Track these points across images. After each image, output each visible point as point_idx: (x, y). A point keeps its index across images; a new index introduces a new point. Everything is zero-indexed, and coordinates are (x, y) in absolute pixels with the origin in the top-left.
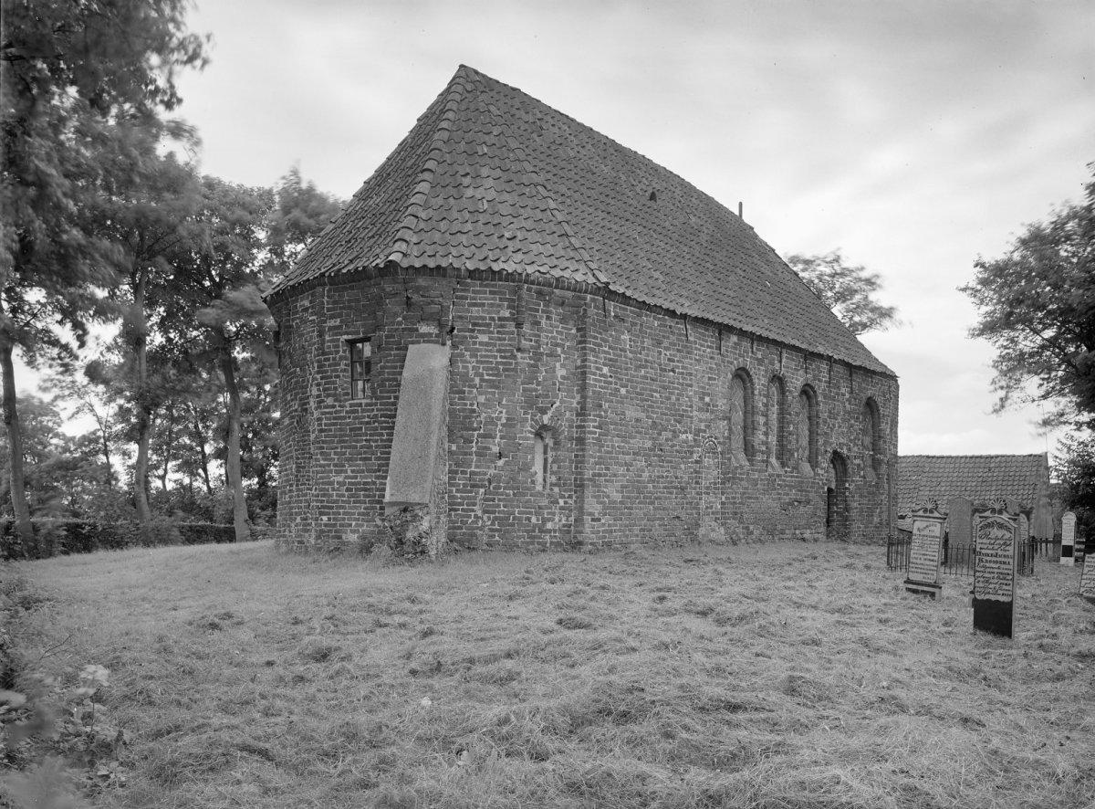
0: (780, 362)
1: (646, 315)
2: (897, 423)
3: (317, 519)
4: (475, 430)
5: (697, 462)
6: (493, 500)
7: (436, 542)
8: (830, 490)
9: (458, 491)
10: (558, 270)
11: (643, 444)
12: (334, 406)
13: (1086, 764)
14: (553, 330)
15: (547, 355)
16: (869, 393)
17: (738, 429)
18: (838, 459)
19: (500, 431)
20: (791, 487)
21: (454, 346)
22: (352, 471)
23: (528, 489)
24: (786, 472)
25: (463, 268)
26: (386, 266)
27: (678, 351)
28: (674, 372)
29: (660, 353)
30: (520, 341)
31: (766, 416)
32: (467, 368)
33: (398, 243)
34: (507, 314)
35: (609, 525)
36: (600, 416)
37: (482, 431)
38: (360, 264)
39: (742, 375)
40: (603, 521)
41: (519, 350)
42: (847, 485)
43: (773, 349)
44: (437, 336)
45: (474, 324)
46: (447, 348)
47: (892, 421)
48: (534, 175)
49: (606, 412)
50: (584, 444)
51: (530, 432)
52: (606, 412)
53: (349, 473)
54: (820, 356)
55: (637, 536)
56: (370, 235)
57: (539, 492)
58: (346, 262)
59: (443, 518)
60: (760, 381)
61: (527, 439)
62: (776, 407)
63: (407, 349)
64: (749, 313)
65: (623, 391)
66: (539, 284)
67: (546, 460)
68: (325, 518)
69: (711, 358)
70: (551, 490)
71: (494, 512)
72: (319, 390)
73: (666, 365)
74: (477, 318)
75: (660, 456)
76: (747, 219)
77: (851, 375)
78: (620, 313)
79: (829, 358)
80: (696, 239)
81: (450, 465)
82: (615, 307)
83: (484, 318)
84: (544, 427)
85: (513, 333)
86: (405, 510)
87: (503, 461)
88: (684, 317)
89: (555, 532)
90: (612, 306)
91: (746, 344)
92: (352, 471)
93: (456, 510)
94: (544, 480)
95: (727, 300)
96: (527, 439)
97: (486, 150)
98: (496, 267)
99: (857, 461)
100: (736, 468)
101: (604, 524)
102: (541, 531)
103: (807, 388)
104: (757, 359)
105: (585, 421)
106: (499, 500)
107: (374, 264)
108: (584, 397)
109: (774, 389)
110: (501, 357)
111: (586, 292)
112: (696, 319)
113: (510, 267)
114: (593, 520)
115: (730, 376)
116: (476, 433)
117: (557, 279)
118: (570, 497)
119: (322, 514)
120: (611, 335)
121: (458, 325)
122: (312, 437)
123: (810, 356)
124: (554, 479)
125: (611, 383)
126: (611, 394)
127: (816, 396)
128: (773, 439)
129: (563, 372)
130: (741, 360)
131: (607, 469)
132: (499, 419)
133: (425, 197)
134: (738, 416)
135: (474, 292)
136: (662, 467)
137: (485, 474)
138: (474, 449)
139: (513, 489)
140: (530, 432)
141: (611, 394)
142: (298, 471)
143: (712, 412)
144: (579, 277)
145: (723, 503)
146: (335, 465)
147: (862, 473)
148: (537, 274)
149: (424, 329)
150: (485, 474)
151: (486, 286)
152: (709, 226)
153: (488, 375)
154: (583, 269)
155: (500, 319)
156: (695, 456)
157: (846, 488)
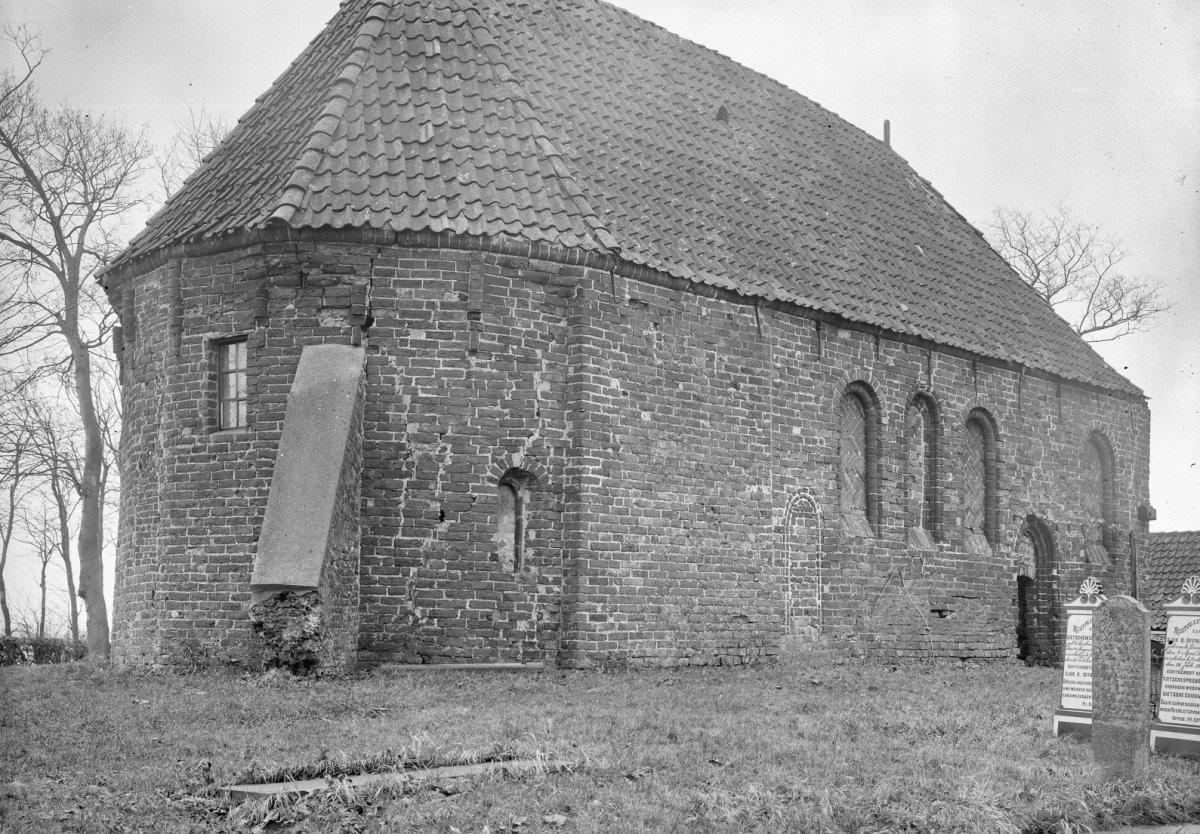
0: (928, 372)
1: (687, 298)
2: (1147, 472)
3: (164, 615)
4: (402, 476)
5: (778, 530)
6: (431, 585)
7: (337, 650)
8: (1023, 581)
9: (376, 571)
10: (536, 229)
11: (681, 499)
12: (192, 441)
13: (5, 669)
14: (526, 316)
15: (519, 361)
16: (1094, 424)
17: (853, 481)
18: (1038, 532)
19: (443, 478)
20: (951, 574)
21: (373, 348)
22: (217, 541)
23: (487, 568)
24: (941, 548)
25: (387, 227)
26: (268, 228)
27: (743, 354)
28: (736, 387)
29: (711, 358)
30: (474, 339)
31: (903, 458)
32: (392, 381)
33: (289, 193)
34: (455, 298)
35: (622, 627)
36: (607, 456)
37: (414, 479)
38: (231, 224)
39: (861, 395)
40: (611, 620)
41: (473, 352)
42: (1055, 573)
43: (915, 351)
44: (347, 332)
45: (404, 314)
46: (361, 352)
47: (1138, 470)
48: (513, 86)
49: (616, 448)
50: (579, 499)
51: (491, 480)
52: (616, 448)
53: (212, 543)
54: (1002, 363)
55: (670, 645)
56: (253, 179)
57: (508, 575)
58: (213, 222)
59: (351, 613)
60: (891, 402)
61: (489, 490)
62: (923, 444)
63: (300, 351)
64: (875, 295)
65: (646, 416)
66: (505, 251)
67: (518, 524)
68: (175, 613)
69: (804, 365)
70: (528, 570)
71: (432, 604)
72: (171, 416)
73: (722, 376)
74: (407, 304)
75: (711, 519)
76: (898, 145)
77: (1058, 394)
78: (639, 293)
79: (1018, 367)
80: (793, 180)
81: (364, 530)
82: (632, 285)
83: (419, 305)
84: (515, 473)
85: (462, 327)
86: (282, 597)
87: (446, 523)
88: (755, 300)
89: (531, 635)
90: (629, 288)
91: (866, 343)
92: (217, 541)
93: (372, 601)
94: (517, 555)
95: (833, 273)
96: (489, 490)
97: (438, 49)
98: (437, 226)
99: (1074, 534)
100: (851, 541)
101: (612, 626)
102: (507, 634)
103: (979, 414)
104: (887, 367)
105: (579, 463)
106: (441, 585)
107: (251, 224)
108: (579, 425)
109: (918, 416)
110: (446, 364)
111: (580, 263)
112: (778, 304)
113: (462, 226)
114: (593, 618)
115: (837, 393)
116: (405, 481)
117: (536, 243)
118: (557, 582)
119: (171, 607)
120: (625, 330)
121: (378, 314)
122: (161, 487)
123: (978, 361)
124: (530, 552)
125: (624, 404)
126: (624, 421)
127: (995, 427)
128: (917, 495)
129: (546, 387)
130: (857, 368)
131: (620, 538)
132: (441, 459)
133: (337, 121)
134: (854, 459)
135: (404, 264)
136: (715, 536)
137: (419, 544)
138: (402, 506)
139: (461, 567)
140: (491, 480)
141: (624, 421)
142: (140, 542)
143: (806, 451)
144: (570, 240)
145: (824, 597)
146: (192, 532)
147: (1082, 554)
148: (502, 235)
149: (328, 320)
150: (419, 544)
151: (424, 255)
152: (821, 159)
153: (425, 391)
154: (579, 226)
155: (443, 305)
156: (776, 521)
157: (1053, 578)
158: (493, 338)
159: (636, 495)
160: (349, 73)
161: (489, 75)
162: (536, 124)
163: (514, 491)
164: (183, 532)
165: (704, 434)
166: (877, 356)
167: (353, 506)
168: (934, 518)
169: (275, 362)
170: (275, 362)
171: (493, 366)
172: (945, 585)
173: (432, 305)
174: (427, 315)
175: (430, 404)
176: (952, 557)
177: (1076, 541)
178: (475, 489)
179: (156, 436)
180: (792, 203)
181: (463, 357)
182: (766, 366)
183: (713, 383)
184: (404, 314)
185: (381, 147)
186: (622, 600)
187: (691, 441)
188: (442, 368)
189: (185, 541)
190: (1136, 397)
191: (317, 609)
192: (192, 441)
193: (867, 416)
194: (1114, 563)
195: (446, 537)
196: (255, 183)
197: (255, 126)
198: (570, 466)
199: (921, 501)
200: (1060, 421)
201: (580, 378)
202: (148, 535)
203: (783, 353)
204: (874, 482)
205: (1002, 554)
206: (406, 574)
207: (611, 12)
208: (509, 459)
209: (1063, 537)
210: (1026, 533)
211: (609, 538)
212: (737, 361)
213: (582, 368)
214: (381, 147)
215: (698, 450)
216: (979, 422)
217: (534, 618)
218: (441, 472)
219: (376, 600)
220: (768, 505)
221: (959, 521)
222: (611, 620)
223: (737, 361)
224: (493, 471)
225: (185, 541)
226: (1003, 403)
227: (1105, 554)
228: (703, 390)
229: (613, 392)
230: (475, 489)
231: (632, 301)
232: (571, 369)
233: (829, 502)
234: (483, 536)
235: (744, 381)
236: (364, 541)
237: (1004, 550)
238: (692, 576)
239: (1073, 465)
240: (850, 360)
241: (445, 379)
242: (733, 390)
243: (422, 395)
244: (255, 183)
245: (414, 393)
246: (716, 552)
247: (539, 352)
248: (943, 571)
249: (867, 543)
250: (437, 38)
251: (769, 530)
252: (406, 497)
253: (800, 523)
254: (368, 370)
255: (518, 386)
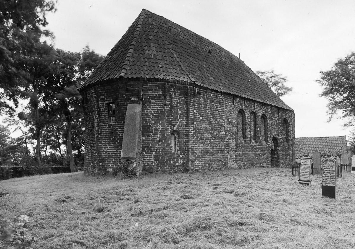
0: (254, 107)
5: (227, 141)
6: (158, 156)
7: (139, 171)
9: (146, 153)
12: (103, 126)
15: (175, 106)
16: (285, 117)
19: (160, 133)
22: (110, 147)
25: (145, 78)
28: (218, 111)
29: (213, 105)
30: (165, 102)
36: (193, 127)
37: (153, 133)
40: (195, 162)
42: (278, 148)
45: (150, 97)
48: (169, 46)
50: (188, 136)
51: (170, 133)
53: (109, 148)
56: (113, 67)
59: (141, 163)
60: (247, 114)
62: (253, 122)
63: (127, 105)
64: (243, 91)
65: (201, 118)
66: (171, 82)
67: (175, 142)
70: (177, 152)
71: (158, 160)
73: (215, 109)
74: (150, 94)
79: (271, 105)
83: (153, 95)
84: (174, 131)
94: (175, 149)
96: (169, 135)
98: (157, 77)
100: (240, 143)
103: (263, 116)
104: (246, 106)
106: (160, 156)
108: (188, 120)
110: (159, 108)
116: (151, 133)
118: (184, 154)
119: (100, 162)
120: (196, 99)
123: (264, 105)
124: (178, 148)
125: (197, 115)
129: (181, 112)
131: (196, 145)
134: (240, 126)
135: (149, 86)
137: (155, 147)
138: (151, 139)
139: (164, 152)
140: (170, 133)
142: (91, 148)
143: (231, 124)
144: (185, 80)
145: (236, 155)
146: (104, 146)
147: (283, 144)
149: (133, 99)
150: (155, 147)
151: (154, 84)
153: (155, 114)
154: (186, 77)
155: (158, 95)
158: (169, 102)
159: (199, 135)
160: (134, 43)
161: (163, 43)
162: (175, 54)
163: (174, 135)
164: (102, 146)
165: (212, 121)
166: (245, 104)
167: (141, 139)
168: (256, 138)
169: (122, 108)
170: (122, 108)
171: (169, 108)
172: (258, 152)
173: (156, 95)
174: (155, 97)
175: (156, 117)
176: (259, 146)
177: (282, 141)
178: (166, 135)
179: (94, 125)
180: (225, 71)
181: (163, 106)
182: (224, 106)
183: (214, 110)
184: (150, 97)
185: (142, 59)
186: (197, 158)
187: (210, 123)
188: (158, 108)
189: (102, 148)
190: (291, 111)
191: (136, 162)
192: (103, 126)
193: (242, 116)
194: (289, 145)
195: (160, 145)
196: (115, 68)
197: (111, 56)
198: (186, 129)
199: (253, 134)
200: (279, 116)
201: (188, 110)
202: (93, 146)
203: (227, 103)
204: (244, 130)
205: (268, 145)
206: (152, 154)
207: (179, 26)
208: (173, 128)
209: (280, 141)
210: (273, 140)
211: (194, 145)
212: (218, 106)
213: (188, 108)
214: (142, 59)
215: (211, 125)
216: (264, 117)
217: (180, 162)
218: (159, 131)
219: (146, 160)
220: (225, 136)
221: (260, 138)
222: (195, 162)
223: (218, 106)
224: (170, 131)
225: (102, 148)
226: (268, 113)
227: (287, 144)
228: (212, 112)
229: (194, 113)
230: (166, 135)
231: (197, 93)
232: (186, 108)
233: (236, 135)
234: (169, 145)
235: (219, 110)
236: (143, 147)
237: (269, 144)
238: (211, 152)
239: (281, 125)
240: (239, 104)
241: (159, 111)
242: (217, 112)
243: (154, 115)
244: (115, 68)
245: (153, 114)
246: (215, 147)
247: (179, 105)
248: (257, 149)
249: (243, 143)
250: (152, 35)
251: (225, 142)
252: (152, 137)
253: (231, 140)
254: (143, 109)
255: (175, 112)
